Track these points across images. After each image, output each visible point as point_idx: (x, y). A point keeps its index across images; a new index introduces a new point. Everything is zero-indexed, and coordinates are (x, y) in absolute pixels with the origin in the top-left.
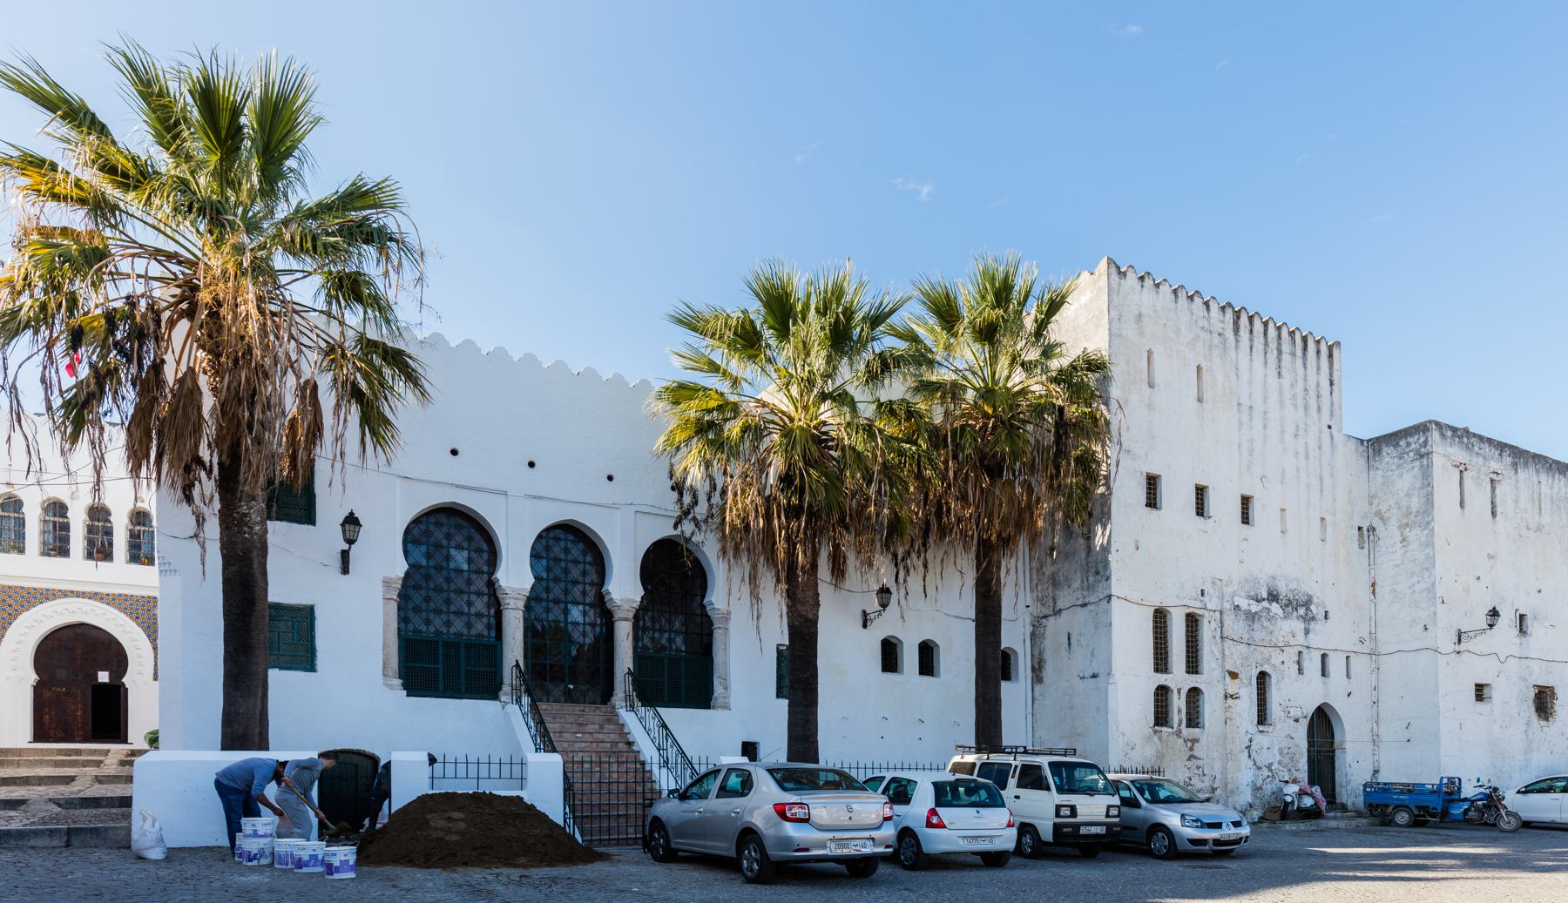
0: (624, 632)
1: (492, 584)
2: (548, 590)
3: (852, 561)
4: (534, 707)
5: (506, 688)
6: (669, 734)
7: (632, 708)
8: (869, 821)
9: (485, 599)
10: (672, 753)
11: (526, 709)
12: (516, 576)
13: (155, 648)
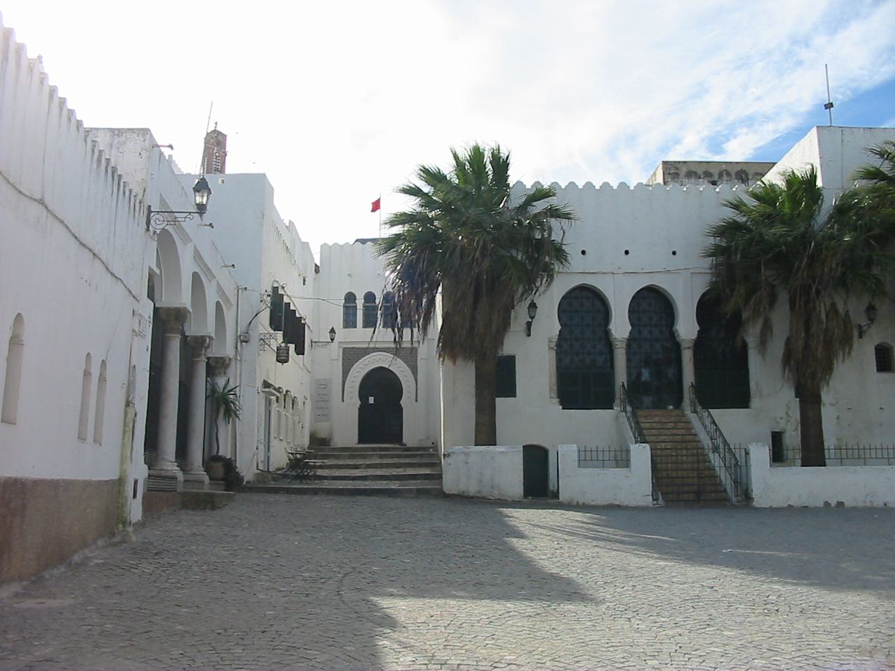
0: (687, 357)
1: (607, 333)
2: (640, 332)
3: (392, 255)
4: (634, 414)
5: (617, 401)
6: (717, 429)
7: (695, 412)
8: (10, 180)
9: (603, 342)
10: (719, 441)
11: (629, 414)
12: (620, 327)
13: (416, 381)
